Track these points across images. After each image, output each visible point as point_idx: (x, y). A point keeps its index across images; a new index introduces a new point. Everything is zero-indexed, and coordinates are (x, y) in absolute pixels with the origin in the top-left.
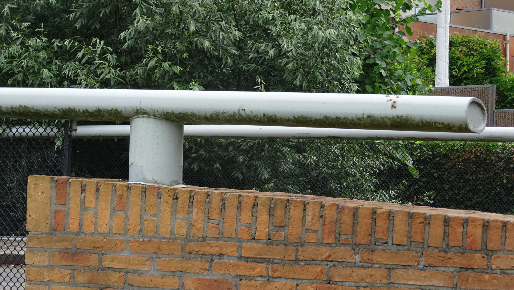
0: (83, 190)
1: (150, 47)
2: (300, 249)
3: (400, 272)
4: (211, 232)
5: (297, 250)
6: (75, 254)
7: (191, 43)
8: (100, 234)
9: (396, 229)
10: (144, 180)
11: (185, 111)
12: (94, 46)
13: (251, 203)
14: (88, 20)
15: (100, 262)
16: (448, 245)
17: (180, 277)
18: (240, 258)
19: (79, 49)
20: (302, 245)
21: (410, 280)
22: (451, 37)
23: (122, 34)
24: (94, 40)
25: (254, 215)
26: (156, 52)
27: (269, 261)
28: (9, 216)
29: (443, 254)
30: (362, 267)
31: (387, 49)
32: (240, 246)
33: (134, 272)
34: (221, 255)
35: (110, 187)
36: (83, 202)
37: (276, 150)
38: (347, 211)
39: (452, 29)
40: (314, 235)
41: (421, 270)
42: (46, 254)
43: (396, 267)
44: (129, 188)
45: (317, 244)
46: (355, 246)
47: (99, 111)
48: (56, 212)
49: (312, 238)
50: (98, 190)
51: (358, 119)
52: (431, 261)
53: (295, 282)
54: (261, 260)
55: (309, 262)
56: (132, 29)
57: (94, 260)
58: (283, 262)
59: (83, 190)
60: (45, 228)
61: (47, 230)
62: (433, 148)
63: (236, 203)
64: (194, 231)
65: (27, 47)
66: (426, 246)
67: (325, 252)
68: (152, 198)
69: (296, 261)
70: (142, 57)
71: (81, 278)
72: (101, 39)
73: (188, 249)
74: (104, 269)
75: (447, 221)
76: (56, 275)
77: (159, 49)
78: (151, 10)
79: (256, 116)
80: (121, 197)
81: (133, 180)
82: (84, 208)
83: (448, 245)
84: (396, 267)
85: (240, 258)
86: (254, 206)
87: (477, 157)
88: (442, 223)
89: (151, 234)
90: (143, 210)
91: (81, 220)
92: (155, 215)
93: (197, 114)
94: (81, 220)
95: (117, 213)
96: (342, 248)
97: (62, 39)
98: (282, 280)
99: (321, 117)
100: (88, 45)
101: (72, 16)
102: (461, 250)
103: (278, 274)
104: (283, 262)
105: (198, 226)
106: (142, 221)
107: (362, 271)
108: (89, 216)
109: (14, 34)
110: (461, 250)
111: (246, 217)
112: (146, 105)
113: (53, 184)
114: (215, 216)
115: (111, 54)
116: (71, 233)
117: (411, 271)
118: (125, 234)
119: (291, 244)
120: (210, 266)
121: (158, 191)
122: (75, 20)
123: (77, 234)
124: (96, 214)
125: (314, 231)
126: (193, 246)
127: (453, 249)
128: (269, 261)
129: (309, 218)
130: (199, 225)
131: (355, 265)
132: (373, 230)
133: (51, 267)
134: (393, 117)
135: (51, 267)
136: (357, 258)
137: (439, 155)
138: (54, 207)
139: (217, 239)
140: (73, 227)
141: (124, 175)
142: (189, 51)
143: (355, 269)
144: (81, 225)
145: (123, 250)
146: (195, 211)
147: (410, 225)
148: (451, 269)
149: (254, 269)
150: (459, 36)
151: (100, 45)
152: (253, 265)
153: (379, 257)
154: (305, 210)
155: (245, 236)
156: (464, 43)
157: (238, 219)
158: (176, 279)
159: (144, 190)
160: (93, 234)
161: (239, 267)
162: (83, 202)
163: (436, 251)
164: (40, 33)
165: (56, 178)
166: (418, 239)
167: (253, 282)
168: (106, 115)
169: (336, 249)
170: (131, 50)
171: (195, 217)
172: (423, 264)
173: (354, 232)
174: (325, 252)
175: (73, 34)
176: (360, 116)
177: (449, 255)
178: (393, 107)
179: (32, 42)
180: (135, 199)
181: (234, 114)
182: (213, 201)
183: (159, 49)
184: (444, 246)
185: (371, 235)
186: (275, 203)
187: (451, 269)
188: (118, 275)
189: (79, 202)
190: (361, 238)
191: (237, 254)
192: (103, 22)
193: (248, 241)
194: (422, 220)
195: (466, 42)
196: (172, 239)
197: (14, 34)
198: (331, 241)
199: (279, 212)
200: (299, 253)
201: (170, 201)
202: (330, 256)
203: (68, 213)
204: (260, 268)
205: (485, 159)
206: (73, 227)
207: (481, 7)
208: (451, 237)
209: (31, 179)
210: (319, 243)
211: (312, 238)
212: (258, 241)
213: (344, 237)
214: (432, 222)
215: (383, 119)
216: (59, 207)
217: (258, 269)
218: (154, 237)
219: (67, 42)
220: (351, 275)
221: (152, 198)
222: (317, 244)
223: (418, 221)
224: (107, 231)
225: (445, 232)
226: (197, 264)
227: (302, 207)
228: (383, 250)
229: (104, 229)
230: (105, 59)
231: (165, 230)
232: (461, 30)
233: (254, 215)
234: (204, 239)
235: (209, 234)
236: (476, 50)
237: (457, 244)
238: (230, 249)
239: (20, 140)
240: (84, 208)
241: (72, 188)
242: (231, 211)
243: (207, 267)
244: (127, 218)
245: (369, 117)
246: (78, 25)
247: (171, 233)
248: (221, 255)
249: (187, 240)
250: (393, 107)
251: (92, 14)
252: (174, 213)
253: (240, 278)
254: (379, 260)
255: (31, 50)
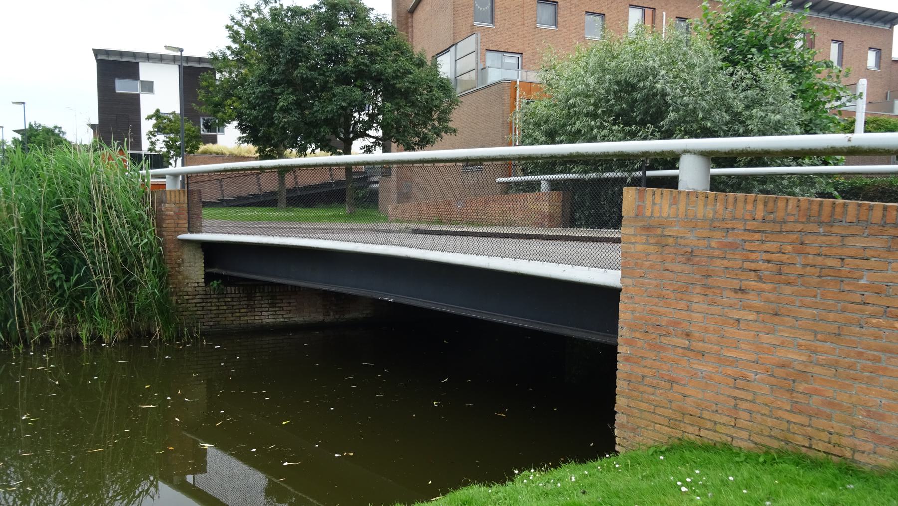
0: (654, 194)
1: (678, 128)
2: (784, 225)
3: (850, 238)
4: (728, 215)
5: (781, 226)
6: (648, 228)
7: (700, 124)
8: (663, 217)
9: (848, 213)
10: (688, 188)
11: (712, 149)
12: (648, 128)
13: (753, 199)
14: (644, 115)
15: (662, 232)
16: (885, 222)
17: (709, 240)
18: (745, 230)
19: (640, 130)
20: (785, 223)
21: (857, 243)
22: (866, 119)
23: (661, 123)
24: (648, 125)
25: (755, 206)
26: (681, 131)
27: (763, 232)
28: (601, 218)
29: (881, 228)
30: (824, 235)
31: (824, 124)
32: (745, 223)
33: (681, 237)
34: (733, 228)
35: (669, 192)
36: (653, 200)
37: (749, 183)
38: (815, 203)
39: (866, 114)
40: (792, 217)
41: (865, 237)
42: (633, 228)
43: (848, 235)
44: (680, 192)
45: (794, 222)
46: (820, 223)
47: (663, 152)
48: (638, 206)
49: (792, 219)
50: (662, 194)
51: (825, 149)
52: (872, 232)
53: (779, 244)
54: (759, 231)
55: (788, 232)
56: (667, 120)
57: (659, 231)
58: (772, 232)
59: (654, 194)
60: (632, 214)
61: (633, 215)
62: (852, 184)
63: (744, 199)
64: (717, 215)
65: (612, 131)
66: (869, 223)
67: (800, 226)
68: (693, 198)
69: (781, 232)
70: (674, 134)
71: (652, 241)
72: (652, 125)
73: (714, 225)
74: (664, 236)
75: (885, 208)
76: (638, 239)
77: (683, 129)
78: (678, 108)
79: (757, 151)
80: (675, 197)
81: (680, 189)
82: (654, 204)
83: (885, 222)
84: (848, 235)
85: (745, 230)
86: (754, 201)
87: (883, 188)
88: (881, 209)
89: (692, 217)
90: (688, 204)
91: (652, 210)
92: (694, 207)
93: (720, 150)
94: (652, 210)
95: (673, 206)
96: (811, 224)
97: (630, 126)
98: (771, 242)
99: (799, 149)
100: (645, 128)
101: (634, 114)
102: (894, 225)
103: (769, 239)
104: (772, 232)
105: (720, 212)
106: (687, 210)
107: (824, 238)
108: (656, 208)
109: (606, 124)
110: (894, 225)
111: (749, 207)
112: (690, 147)
113: (637, 191)
114: (731, 207)
115: (657, 132)
116: (646, 217)
117: (857, 238)
118: (677, 217)
119: (778, 222)
120: (727, 235)
121: (697, 194)
122: (636, 116)
123: (650, 217)
124: (661, 206)
125: (793, 215)
126: (717, 224)
127: (889, 225)
128: (763, 232)
129: (790, 207)
130: (721, 211)
131: (819, 234)
132: (832, 213)
133: (635, 235)
134: (849, 147)
135: (635, 235)
136: (821, 230)
137: (856, 187)
138: (637, 203)
139: (731, 220)
140: (648, 213)
141: (677, 188)
142: (700, 128)
143: (819, 236)
144: (652, 213)
145: (675, 226)
146: (718, 204)
147: (858, 210)
148: (886, 237)
149: (754, 236)
150: (871, 118)
151: (651, 128)
152: (753, 234)
153: (836, 229)
154: (787, 203)
155: (749, 218)
156: (874, 122)
157: (744, 208)
158: (706, 242)
159: (689, 193)
160: (659, 217)
161: (744, 234)
162: (653, 200)
163: (876, 226)
164: (619, 123)
165: (638, 188)
166: (864, 218)
167: (753, 243)
168: (666, 154)
169: (807, 225)
170: (666, 131)
171: (718, 208)
172: (866, 233)
173: (819, 215)
174: (800, 226)
175: (636, 123)
176: (825, 147)
177: (885, 228)
178: (849, 140)
179: (615, 127)
180: (683, 198)
181: (743, 150)
182: (730, 199)
183: (683, 129)
184: (882, 223)
185: (831, 217)
186: (768, 199)
187: (886, 237)
188: (672, 239)
189: (651, 200)
190: (825, 217)
191: (743, 228)
192: (651, 116)
193: (750, 220)
194: (867, 207)
195: (875, 121)
196: (705, 219)
197: (606, 124)
198: (803, 220)
199: (771, 204)
200: (783, 227)
201: (704, 198)
202: (802, 229)
203: (645, 207)
204: (757, 236)
205: (888, 190)
206: (648, 213)
207: (886, 99)
208: (887, 217)
209: (625, 189)
210: (796, 221)
211: (792, 219)
212: (757, 220)
213: (812, 218)
214: (874, 208)
215: (841, 148)
216: (640, 203)
217: (756, 236)
218: (693, 219)
219: (633, 127)
220: (816, 240)
221: (693, 198)
222: (794, 222)
223: (865, 208)
224: (667, 215)
225: (883, 214)
226: (718, 234)
227: (786, 201)
228: (839, 225)
229: (665, 214)
230: (654, 135)
231: (700, 215)
232: (872, 114)
233: (755, 206)
234: (723, 219)
235: (727, 216)
236: (882, 126)
237: (892, 221)
238: (739, 225)
239: (608, 179)
240: (654, 204)
241: (648, 193)
242: (740, 204)
243: (725, 234)
244: (678, 209)
245: (832, 147)
246: (638, 119)
247: (704, 216)
248: (733, 228)
249: (713, 220)
250: (849, 140)
251: (646, 113)
252: (706, 205)
253: (745, 241)
254: (836, 231)
255: (614, 132)
